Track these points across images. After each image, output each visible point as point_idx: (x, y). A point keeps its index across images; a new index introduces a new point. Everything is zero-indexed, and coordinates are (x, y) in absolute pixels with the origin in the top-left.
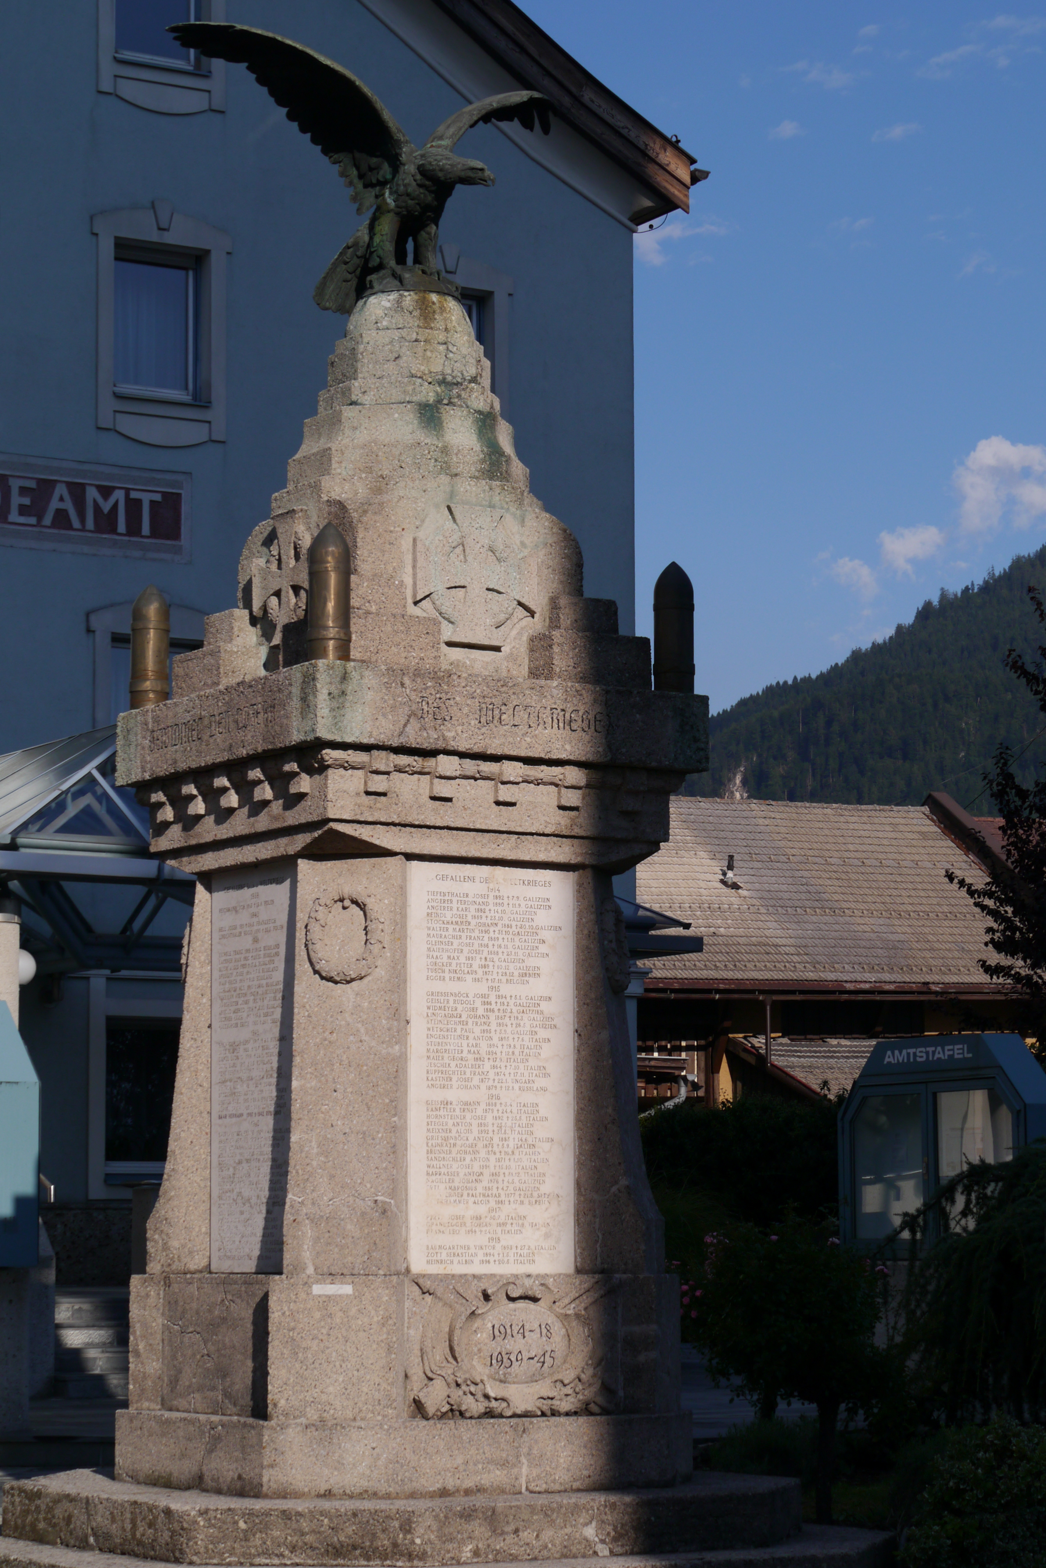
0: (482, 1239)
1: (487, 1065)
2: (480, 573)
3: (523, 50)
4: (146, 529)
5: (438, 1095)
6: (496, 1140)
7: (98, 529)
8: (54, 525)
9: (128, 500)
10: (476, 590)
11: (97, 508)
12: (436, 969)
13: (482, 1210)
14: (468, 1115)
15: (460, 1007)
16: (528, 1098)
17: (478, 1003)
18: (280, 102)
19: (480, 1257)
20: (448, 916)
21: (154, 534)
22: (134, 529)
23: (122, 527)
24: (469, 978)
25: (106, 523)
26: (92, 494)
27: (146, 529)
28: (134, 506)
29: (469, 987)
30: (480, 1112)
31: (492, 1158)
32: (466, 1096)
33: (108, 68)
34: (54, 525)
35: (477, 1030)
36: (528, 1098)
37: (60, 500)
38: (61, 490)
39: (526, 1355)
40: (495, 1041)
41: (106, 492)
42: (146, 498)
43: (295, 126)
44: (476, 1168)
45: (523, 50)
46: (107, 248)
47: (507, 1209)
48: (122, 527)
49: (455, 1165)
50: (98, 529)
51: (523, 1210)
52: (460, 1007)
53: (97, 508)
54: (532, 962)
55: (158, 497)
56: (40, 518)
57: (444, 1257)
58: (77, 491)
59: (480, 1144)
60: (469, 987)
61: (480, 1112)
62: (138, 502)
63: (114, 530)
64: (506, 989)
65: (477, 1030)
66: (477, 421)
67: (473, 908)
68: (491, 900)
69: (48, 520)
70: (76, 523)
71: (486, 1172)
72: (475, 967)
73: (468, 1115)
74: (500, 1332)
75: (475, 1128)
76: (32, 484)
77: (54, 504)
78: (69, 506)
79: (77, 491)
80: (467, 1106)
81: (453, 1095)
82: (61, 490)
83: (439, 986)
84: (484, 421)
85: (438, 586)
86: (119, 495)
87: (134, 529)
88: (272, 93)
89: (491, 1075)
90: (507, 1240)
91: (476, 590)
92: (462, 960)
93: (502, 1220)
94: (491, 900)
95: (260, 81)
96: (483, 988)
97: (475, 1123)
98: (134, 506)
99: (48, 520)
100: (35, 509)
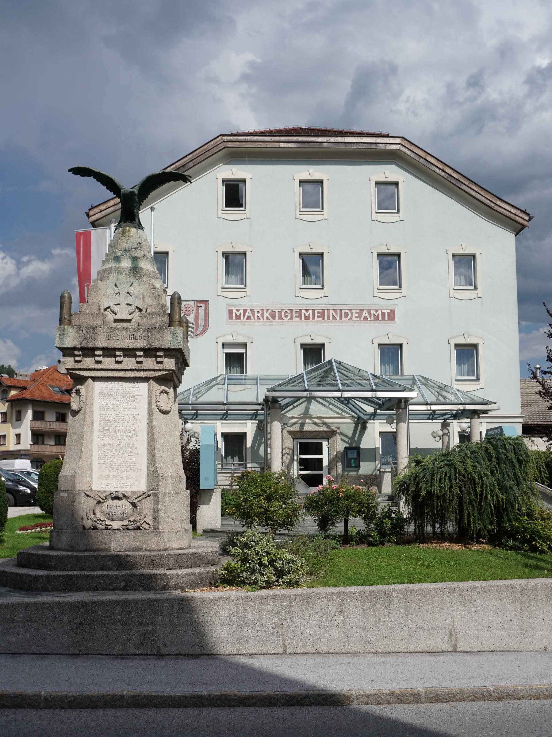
0: (115, 481)
1: (118, 434)
2: (124, 300)
3: (480, 194)
4: (386, 318)
5: (102, 442)
6: (120, 454)
7: (375, 320)
8: (364, 319)
9: (382, 312)
10: (123, 304)
11: (374, 315)
12: (102, 408)
13: (115, 473)
14: (111, 448)
15: (109, 418)
16: (131, 442)
17: (115, 417)
18: (104, 185)
19: (115, 486)
20: (106, 393)
21: (389, 319)
22: (383, 319)
23: (380, 319)
24: (112, 410)
25: (377, 318)
26: (373, 312)
27: (386, 318)
28: (383, 314)
29: (112, 412)
30: (115, 446)
31: (119, 459)
32: (111, 442)
33: (374, 214)
34: (364, 319)
35: (115, 424)
36: (131, 442)
37: (365, 313)
38: (365, 311)
39: (117, 513)
40: (121, 426)
41: (376, 311)
42: (386, 312)
43: (109, 191)
44: (114, 462)
45: (480, 194)
46: (375, 255)
47: (123, 473)
48: (380, 319)
49: (107, 461)
50: (375, 320)
51: (128, 473)
52: (109, 418)
53: (374, 315)
54: (133, 405)
55: (389, 311)
56: (360, 318)
57: (103, 486)
58: (369, 311)
59: (115, 455)
60: (112, 412)
61: (115, 446)
62: (384, 312)
63: (378, 320)
64: (124, 413)
65: (115, 424)
66: (131, 259)
67: (114, 391)
68: (120, 388)
69: (362, 319)
70: (369, 319)
71: (117, 463)
72: (115, 406)
73: (111, 448)
74: (110, 507)
75: (114, 451)
76: (358, 311)
77: (364, 315)
78: (367, 315)
79: (369, 311)
80: (111, 445)
81: (106, 442)
82: (365, 311)
83: (103, 412)
84: (134, 259)
85: (111, 304)
86: (380, 312)
87: (383, 319)
88: (101, 183)
89: (119, 436)
90: (123, 481)
91: (123, 304)
92: (111, 405)
93: (122, 476)
94: (120, 388)
95: (98, 180)
96: (117, 412)
97: (114, 450)
98: (383, 314)
99: (362, 319)
100: (359, 317)
